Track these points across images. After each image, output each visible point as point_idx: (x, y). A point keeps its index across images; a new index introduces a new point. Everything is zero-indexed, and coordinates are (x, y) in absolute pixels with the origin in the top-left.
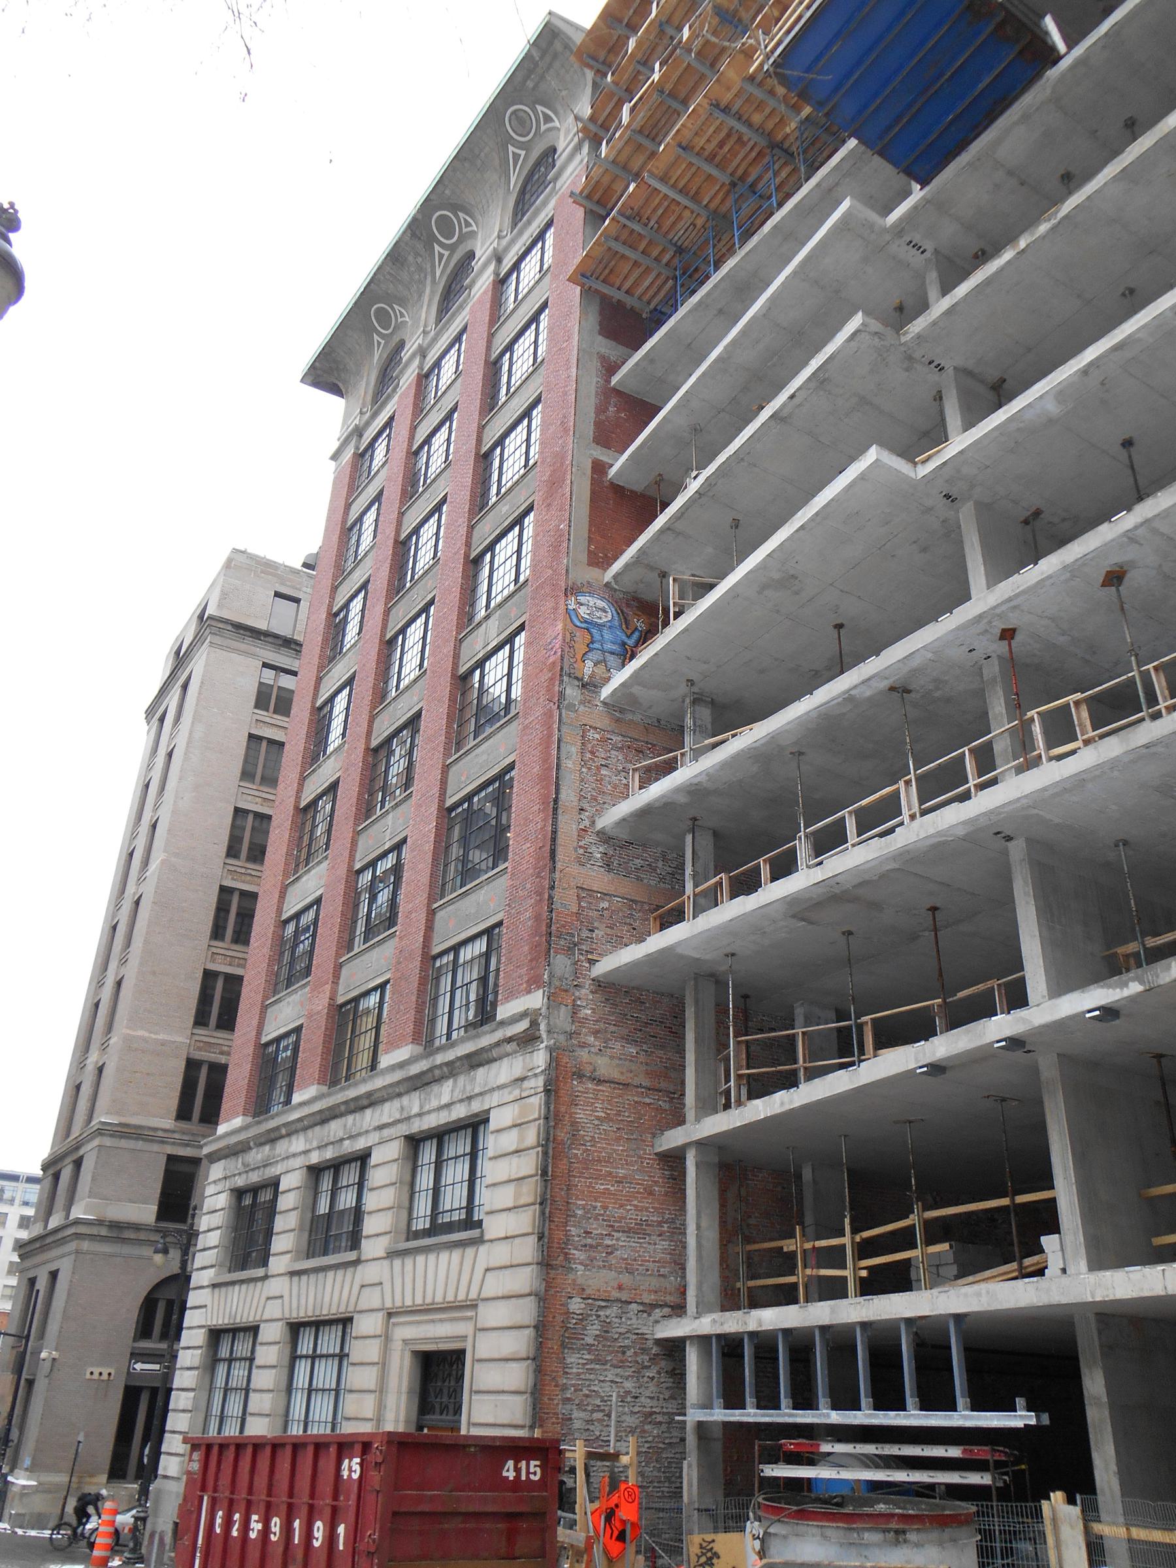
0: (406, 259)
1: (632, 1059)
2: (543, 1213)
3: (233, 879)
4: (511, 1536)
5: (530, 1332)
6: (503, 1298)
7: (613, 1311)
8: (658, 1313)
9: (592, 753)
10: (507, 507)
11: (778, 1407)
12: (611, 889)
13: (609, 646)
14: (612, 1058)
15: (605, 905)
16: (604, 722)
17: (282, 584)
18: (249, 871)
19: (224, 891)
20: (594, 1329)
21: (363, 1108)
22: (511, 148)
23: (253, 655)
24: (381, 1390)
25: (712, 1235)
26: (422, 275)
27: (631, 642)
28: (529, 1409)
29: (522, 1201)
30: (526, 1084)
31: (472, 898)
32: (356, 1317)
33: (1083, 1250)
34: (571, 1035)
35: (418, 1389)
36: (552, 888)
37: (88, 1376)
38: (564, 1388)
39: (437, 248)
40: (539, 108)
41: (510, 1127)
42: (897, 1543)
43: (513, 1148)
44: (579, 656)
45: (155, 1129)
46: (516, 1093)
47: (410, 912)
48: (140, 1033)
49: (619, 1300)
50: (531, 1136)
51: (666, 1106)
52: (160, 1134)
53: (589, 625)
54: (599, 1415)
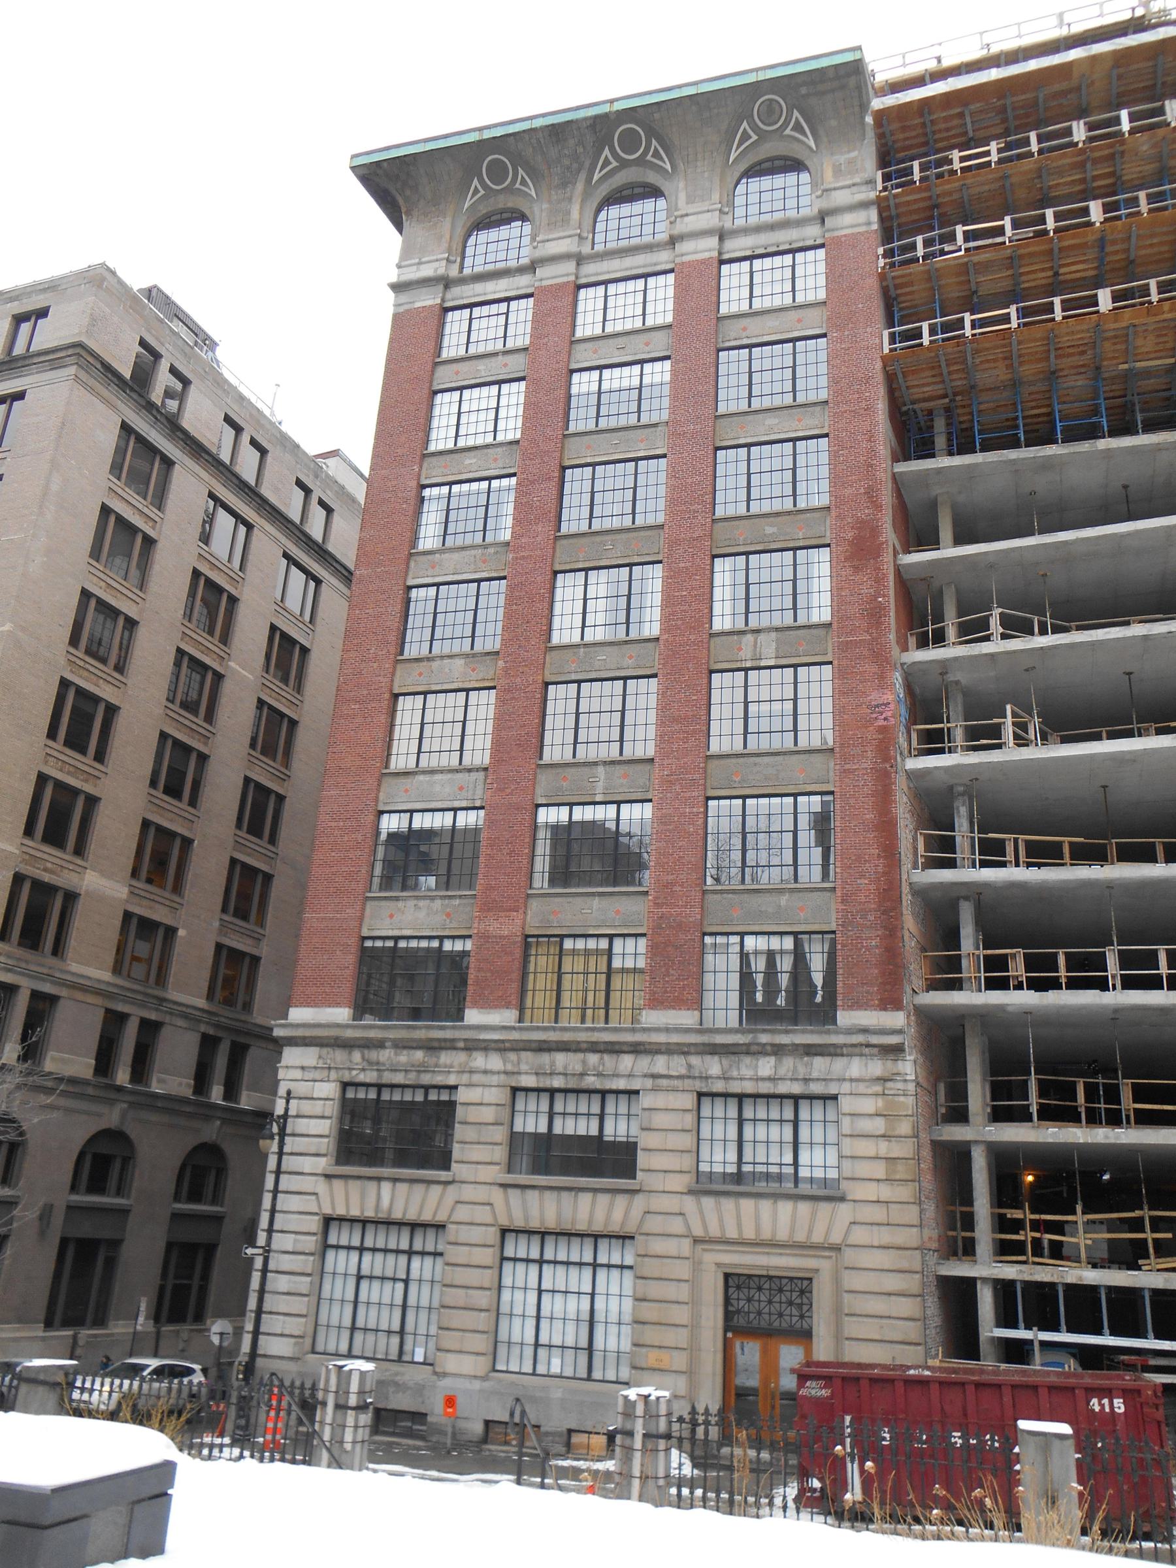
3: (71, 671)
10: (774, 530)
11: (1058, 1331)
18: (87, 666)
22: (745, 124)
23: (114, 407)
24: (694, 1302)
26: (575, 166)
30: (889, 1084)
39: (606, 152)
40: (796, 114)
43: (882, 1132)
46: (878, 1088)
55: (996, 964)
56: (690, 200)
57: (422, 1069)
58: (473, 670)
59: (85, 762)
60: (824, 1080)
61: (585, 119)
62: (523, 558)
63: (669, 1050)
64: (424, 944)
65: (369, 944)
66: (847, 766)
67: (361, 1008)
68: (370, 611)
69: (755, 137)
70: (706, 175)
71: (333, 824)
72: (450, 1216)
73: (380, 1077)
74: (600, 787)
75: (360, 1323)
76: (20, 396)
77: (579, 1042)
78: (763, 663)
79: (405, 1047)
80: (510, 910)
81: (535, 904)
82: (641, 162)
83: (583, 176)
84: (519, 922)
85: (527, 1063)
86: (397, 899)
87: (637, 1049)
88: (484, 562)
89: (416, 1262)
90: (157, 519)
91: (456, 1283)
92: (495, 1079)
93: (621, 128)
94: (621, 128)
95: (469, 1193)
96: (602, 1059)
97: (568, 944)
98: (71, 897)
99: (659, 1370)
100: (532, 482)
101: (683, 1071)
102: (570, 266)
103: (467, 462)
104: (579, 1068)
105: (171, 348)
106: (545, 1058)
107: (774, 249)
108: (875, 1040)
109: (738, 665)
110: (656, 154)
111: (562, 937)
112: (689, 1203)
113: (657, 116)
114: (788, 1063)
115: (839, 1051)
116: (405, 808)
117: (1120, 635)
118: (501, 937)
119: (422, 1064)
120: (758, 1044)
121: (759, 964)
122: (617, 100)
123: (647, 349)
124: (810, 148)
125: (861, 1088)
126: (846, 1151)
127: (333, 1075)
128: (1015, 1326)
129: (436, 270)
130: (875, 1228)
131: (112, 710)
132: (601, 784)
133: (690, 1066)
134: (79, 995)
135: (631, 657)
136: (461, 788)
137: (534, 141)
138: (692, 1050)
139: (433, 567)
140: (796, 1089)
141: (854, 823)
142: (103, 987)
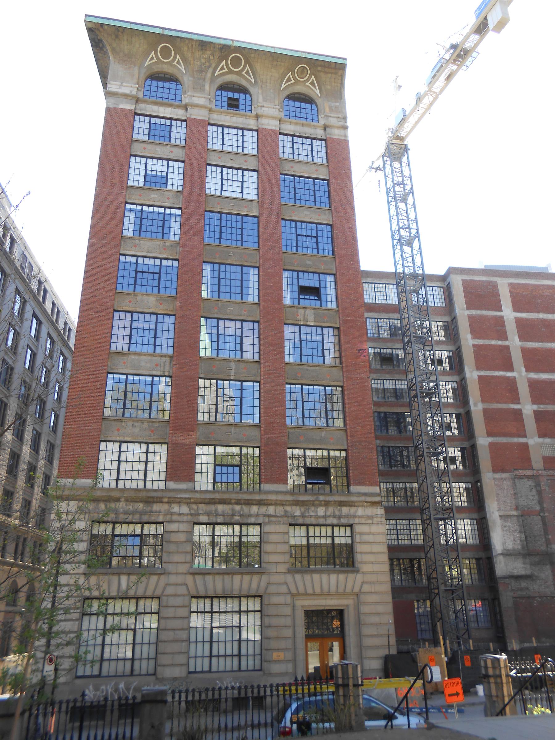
0: (206, 50)
26: (207, 64)
56: (265, 100)
58: (161, 304)
61: (219, 44)
62: (187, 251)
63: (276, 503)
66: (349, 375)
68: (100, 263)
69: (293, 81)
70: (271, 90)
71: (81, 377)
72: (145, 592)
74: (233, 372)
75: (215, 653)
77: (231, 499)
79: (132, 501)
80: (189, 431)
81: (201, 429)
82: (239, 73)
85: (202, 510)
87: (260, 503)
88: (165, 249)
89: (244, 617)
91: (168, 627)
92: (185, 518)
93: (231, 57)
94: (231, 57)
95: (173, 579)
96: (242, 508)
99: (278, 661)
100: (191, 214)
103: (153, 196)
104: (230, 512)
106: (212, 508)
107: (304, 135)
109: (297, 322)
110: (247, 73)
112: (289, 578)
113: (253, 55)
114: (331, 510)
115: (353, 504)
116: (124, 372)
118: (185, 444)
122: (236, 41)
124: (318, 95)
129: (131, 92)
135: (245, 311)
136: (157, 365)
137: (190, 45)
138: (287, 503)
139: (135, 246)
140: (335, 521)
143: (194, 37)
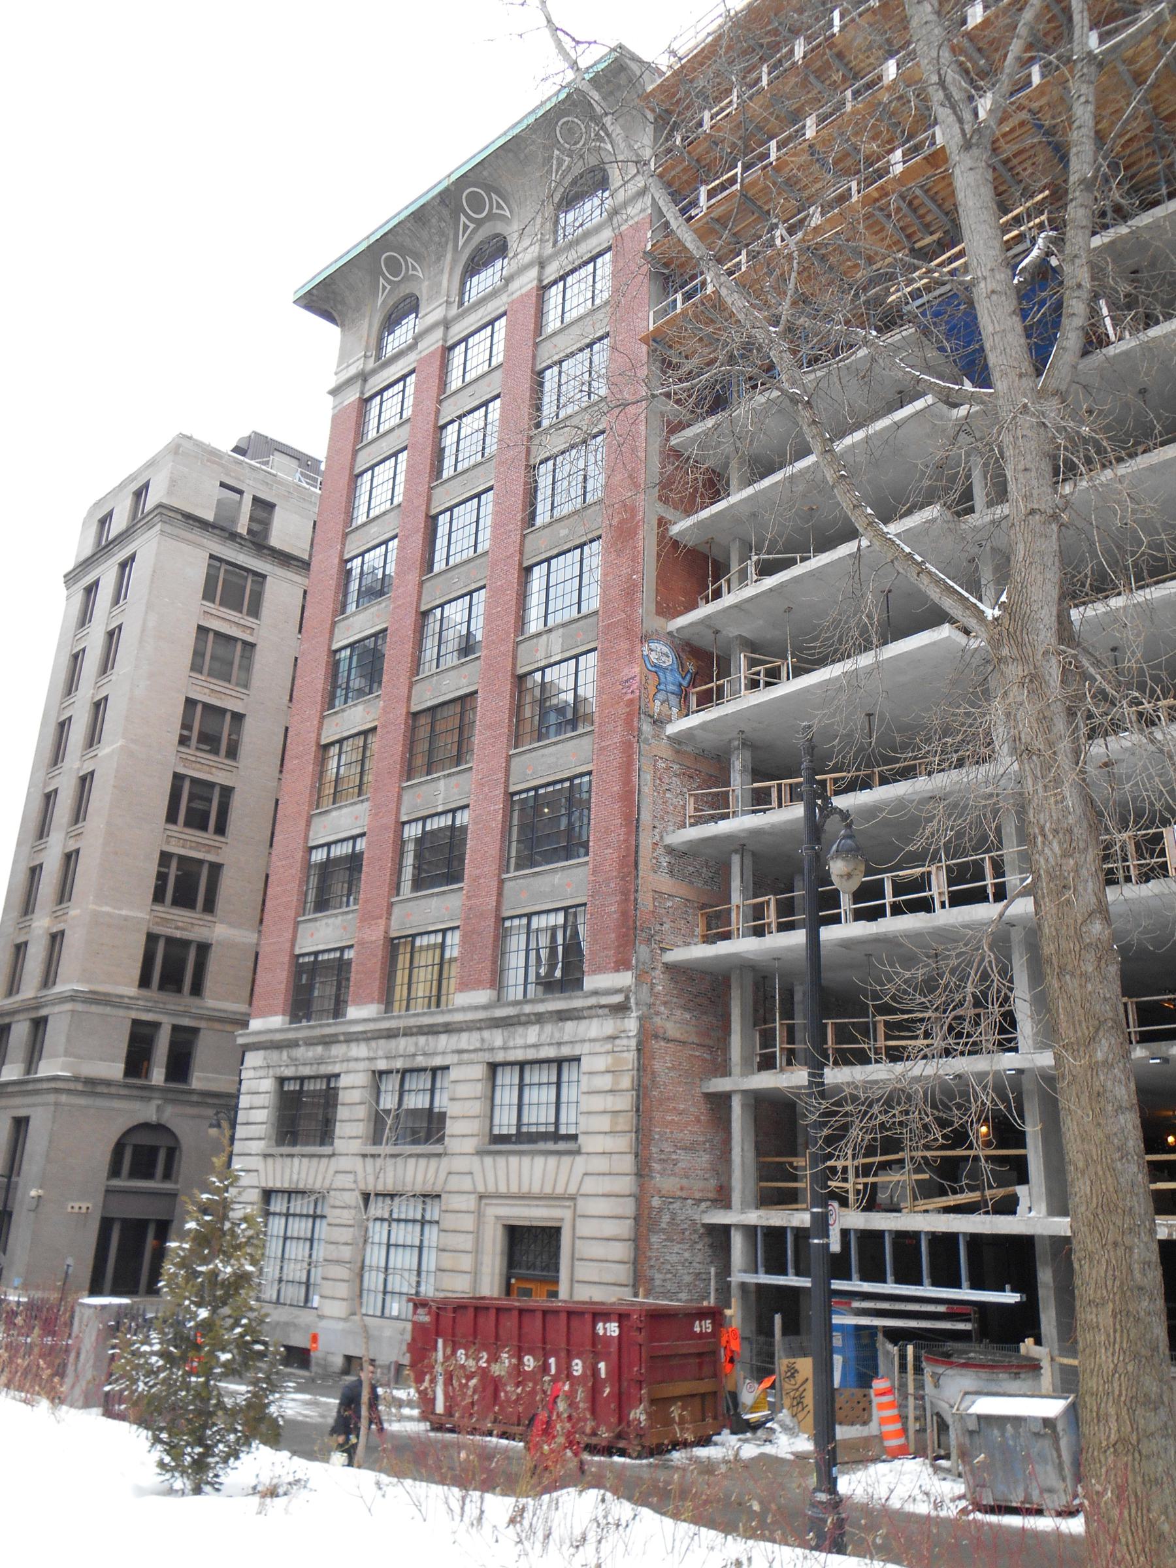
1: (687, 1023)
2: (637, 1139)
4: (700, 1365)
5: (630, 1222)
6: (603, 1195)
7: (677, 1205)
8: (704, 1205)
9: (660, 779)
12: (673, 891)
13: (671, 687)
14: (675, 1022)
15: (670, 904)
16: (667, 753)
17: (227, 474)
19: (178, 778)
20: (666, 1218)
21: (438, 1033)
23: (200, 546)
24: (477, 1251)
25: (750, 1155)
26: (443, 239)
27: (685, 683)
28: (632, 1275)
29: (619, 1129)
30: (617, 1042)
31: (540, 879)
32: (444, 1196)
33: (1044, 1197)
34: (650, 1006)
35: (506, 1250)
36: (636, 891)
37: (69, 1210)
38: (650, 1259)
39: (463, 218)
41: (603, 1072)
42: (1015, 1379)
43: (608, 1088)
44: (651, 697)
45: (122, 997)
46: (609, 1047)
47: (479, 877)
48: (106, 909)
49: (680, 1197)
50: (626, 1082)
51: (708, 1057)
52: (126, 1000)
53: (658, 669)
54: (669, 1276)
55: (758, 912)
57: (320, 1061)
59: (207, 837)
60: (571, 1042)
61: (433, 198)
62: (400, 606)
64: (332, 956)
65: (301, 960)
66: (603, 744)
67: (295, 1018)
73: (297, 1070)
76: (132, 558)
78: (553, 660)
83: (450, 246)
84: (382, 928)
86: (315, 920)
90: (254, 626)
97: (418, 942)
98: (204, 949)
101: (478, 1045)
102: (439, 333)
104: (412, 1050)
105: (251, 483)
106: (393, 1043)
108: (604, 1000)
111: (414, 936)
113: (485, 173)
117: (828, 560)
119: (321, 1057)
120: (525, 1015)
121: (544, 941)
123: (489, 389)
125: (598, 1047)
126: (583, 1107)
127: (271, 1073)
128: (783, 1272)
130: (601, 1178)
131: (227, 792)
132: (441, 796)
133: (483, 1040)
134: (217, 1026)
136: (356, 818)
141: (605, 796)
142: (238, 1017)
143: (402, 217)
